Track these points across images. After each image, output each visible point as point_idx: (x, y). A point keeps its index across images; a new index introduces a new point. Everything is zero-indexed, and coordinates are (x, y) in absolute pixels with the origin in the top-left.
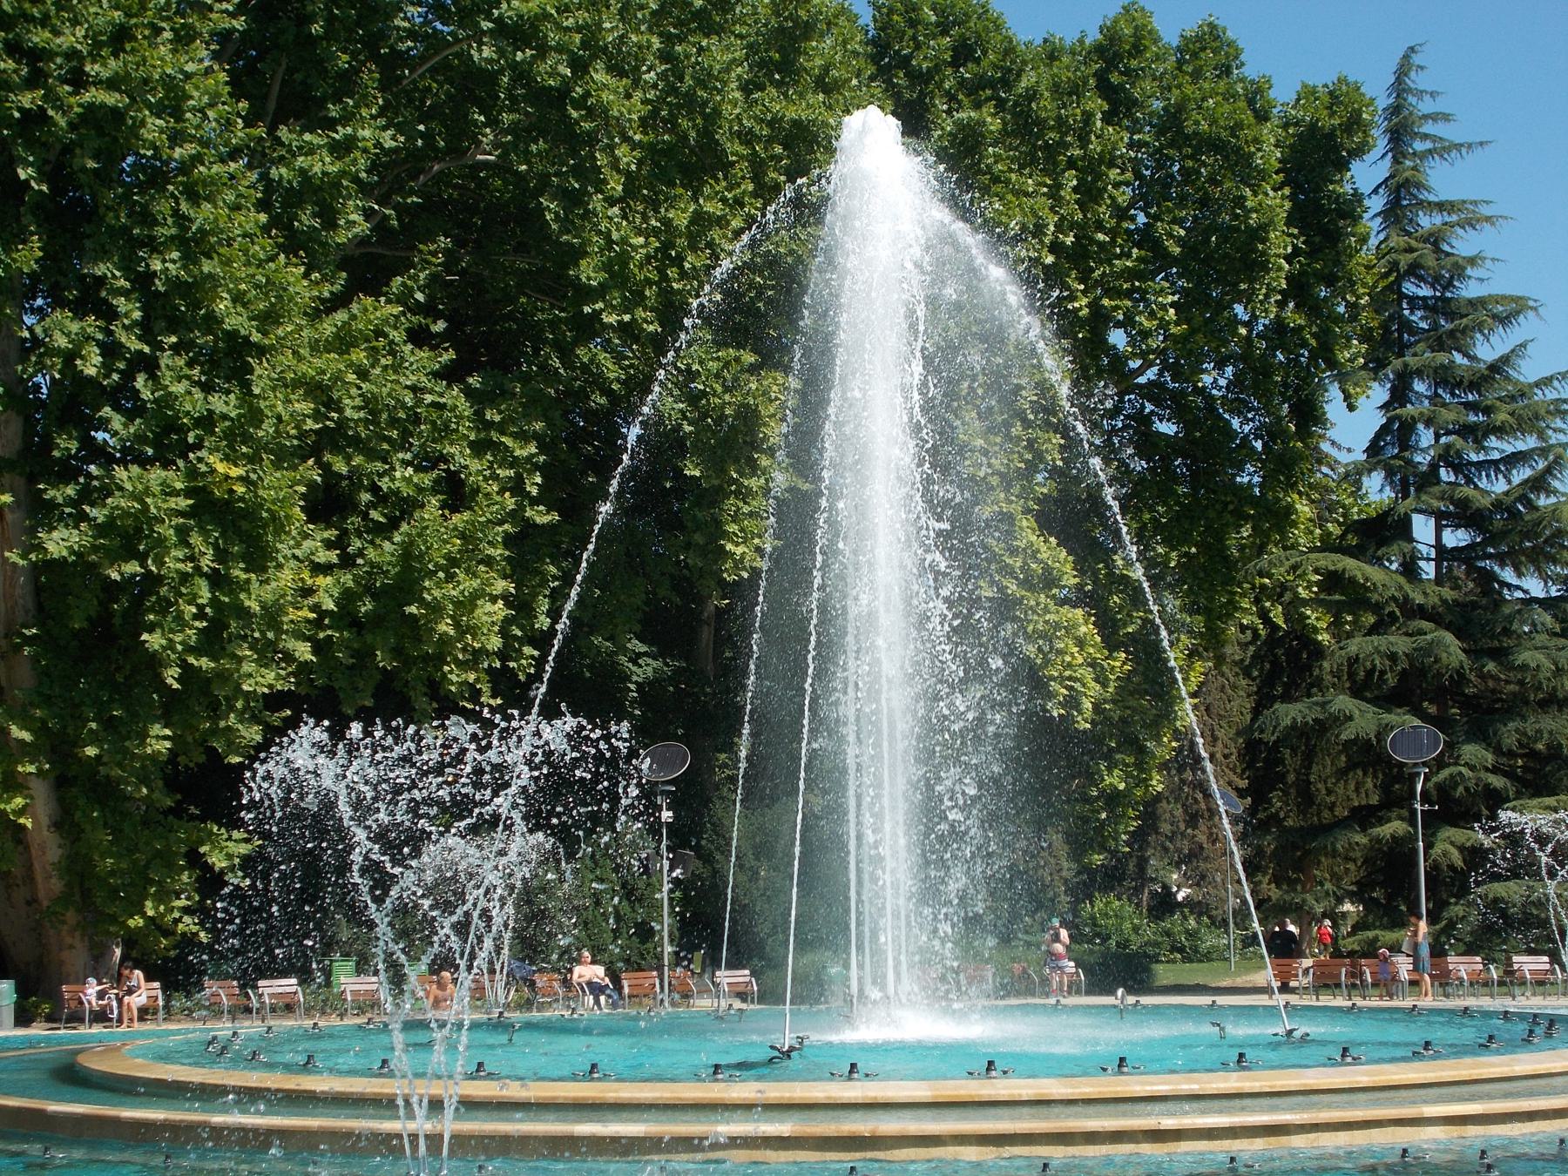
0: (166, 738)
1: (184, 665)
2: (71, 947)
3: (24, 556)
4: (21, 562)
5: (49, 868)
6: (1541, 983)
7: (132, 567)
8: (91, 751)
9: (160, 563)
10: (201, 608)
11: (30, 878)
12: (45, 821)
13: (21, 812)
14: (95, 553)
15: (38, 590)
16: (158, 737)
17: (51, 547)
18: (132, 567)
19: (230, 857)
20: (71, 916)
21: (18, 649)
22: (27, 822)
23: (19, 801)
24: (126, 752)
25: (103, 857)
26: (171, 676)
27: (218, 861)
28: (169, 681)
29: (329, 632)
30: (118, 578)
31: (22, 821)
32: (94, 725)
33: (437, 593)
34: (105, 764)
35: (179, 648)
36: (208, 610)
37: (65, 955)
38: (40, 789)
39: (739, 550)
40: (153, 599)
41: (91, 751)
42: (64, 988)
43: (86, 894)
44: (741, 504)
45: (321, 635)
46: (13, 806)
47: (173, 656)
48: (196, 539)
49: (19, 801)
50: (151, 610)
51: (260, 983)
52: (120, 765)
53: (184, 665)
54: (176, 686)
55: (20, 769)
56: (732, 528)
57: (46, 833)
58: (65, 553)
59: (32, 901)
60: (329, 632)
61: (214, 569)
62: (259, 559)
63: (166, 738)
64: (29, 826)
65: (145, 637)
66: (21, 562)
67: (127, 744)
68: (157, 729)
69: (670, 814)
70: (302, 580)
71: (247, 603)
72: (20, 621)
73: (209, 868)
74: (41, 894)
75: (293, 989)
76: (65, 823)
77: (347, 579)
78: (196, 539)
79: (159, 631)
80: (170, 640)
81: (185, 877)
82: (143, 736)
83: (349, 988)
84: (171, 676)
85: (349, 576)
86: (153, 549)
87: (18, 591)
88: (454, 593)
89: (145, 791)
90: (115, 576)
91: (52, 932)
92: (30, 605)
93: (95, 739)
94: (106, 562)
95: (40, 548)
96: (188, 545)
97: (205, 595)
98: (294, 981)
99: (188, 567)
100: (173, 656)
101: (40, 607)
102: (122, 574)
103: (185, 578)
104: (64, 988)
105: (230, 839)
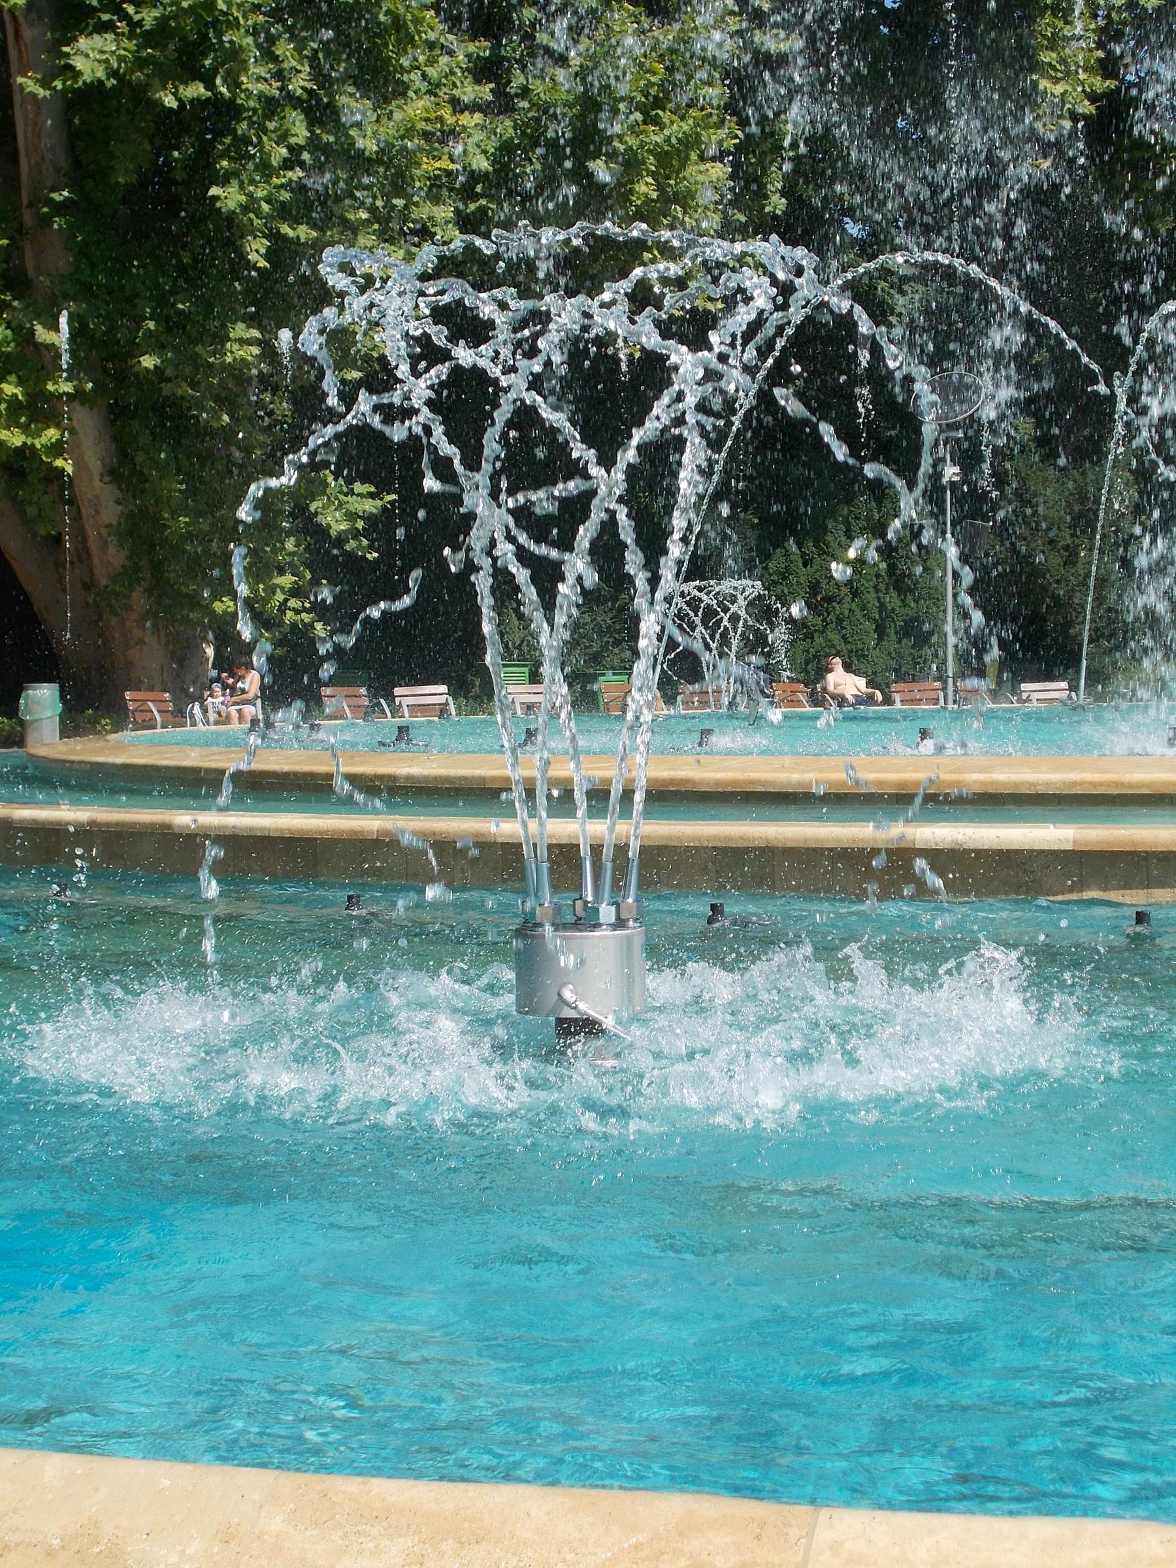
0: (249, 342)
1: (275, 236)
2: (141, 641)
3: (45, 83)
4: (42, 93)
5: (104, 532)
6: (549, 797)
7: (196, 90)
8: (148, 362)
9: (235, 85)
10: (295, 150)
11: (83, 554)
12: (95, 465)
13: (57, 449)
14: (141, 69)
15: (73, 137)
16: (242, 342)
17: (79, 63)
18: (196, 90)
19: (352, 516)
20: (139, 600)
21: (46, 221)
22: (66, 465)
23: (52, 434)
24: (196, 362)
25: (175, 515)
26: (256, 250)
27: (335, 522)
28: (253, 257)
29: (483, 202)
30: (174, 105)
31: (59, 463)
32: (151, 325)
33: (631, 141)
34: (169, 380)
35: (265, 207)
36: (306, 156)
37: (134, 654)
38: (87, 421)
39: (1059, 89)
40: (228, 140)
41: (148, 362)
42: (128, 695)
43: (157, 568)
44: (1060, 24)
45: (472, 207)
46: (44, 440)
47: (257, 222)
48: (284, 48)
49: (52, 434)
50: (225, 154)
51: (398, 691)
52: (194, 385)
53: (275, 236)
54: (262, 263)
55: (50, 387)
56: (1047, 57)
57: (98, 484)
58: (101, 74)
59: (89, 585)
60: (483, 202)
61: (310, 92)
62: (380, 82)
63: (249, 342)
64: (69, 470)
65: (214, 191)
66: (42, 93)
67: (199, 349)
68: (239, 330)
69: (957, 470)
70: (440, 119)
71: (360, 143)
72: (49, 184)
73: (322, 532)
74: (99, 571)
75: (442, 699)
76: (124, 472)
77: (506, 127)
78: (284, 48)
79: (235, 182)
80: (250, 196)
81: (290, 544)
82: (222, 338)
83: (520, 699)
84: (256, 250)
85: (509, 123)
86: (223, 64)
87: (46, 142)
88: (659, 139)
89: (226, 418)
90: (170, 101)
91: (114, 621)
92: (63, 161)
93: (156, 344)
94: (156, 82)
95: (71, 71)
96: (275, 59)
97: (300, 133)
98: (443, 688)
99: (273, 89)
100: (257, 222)
101: (76, 164)
102: (180, 100)
103: (271, 107)
104: (128, 695)
105: (351, 492)
